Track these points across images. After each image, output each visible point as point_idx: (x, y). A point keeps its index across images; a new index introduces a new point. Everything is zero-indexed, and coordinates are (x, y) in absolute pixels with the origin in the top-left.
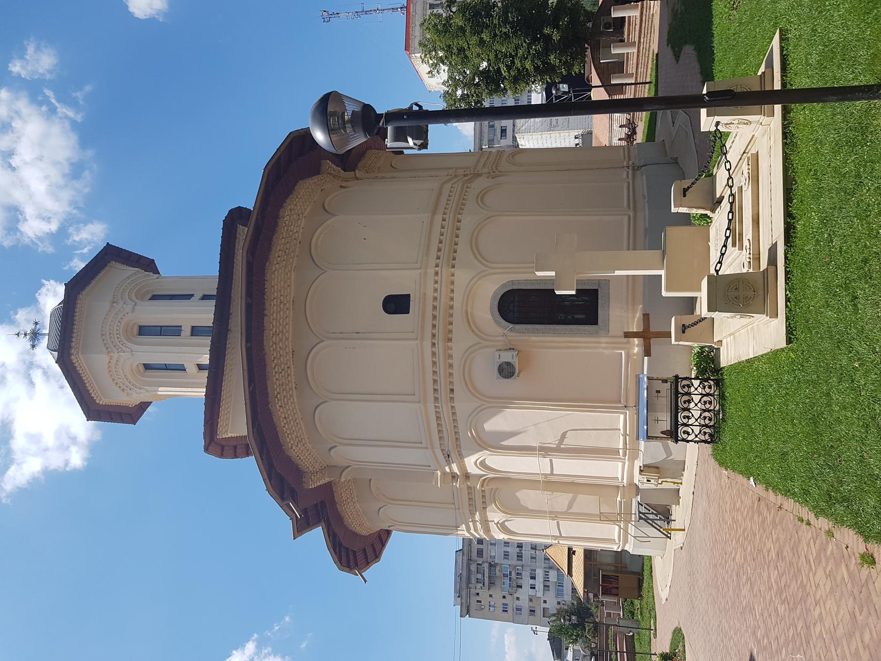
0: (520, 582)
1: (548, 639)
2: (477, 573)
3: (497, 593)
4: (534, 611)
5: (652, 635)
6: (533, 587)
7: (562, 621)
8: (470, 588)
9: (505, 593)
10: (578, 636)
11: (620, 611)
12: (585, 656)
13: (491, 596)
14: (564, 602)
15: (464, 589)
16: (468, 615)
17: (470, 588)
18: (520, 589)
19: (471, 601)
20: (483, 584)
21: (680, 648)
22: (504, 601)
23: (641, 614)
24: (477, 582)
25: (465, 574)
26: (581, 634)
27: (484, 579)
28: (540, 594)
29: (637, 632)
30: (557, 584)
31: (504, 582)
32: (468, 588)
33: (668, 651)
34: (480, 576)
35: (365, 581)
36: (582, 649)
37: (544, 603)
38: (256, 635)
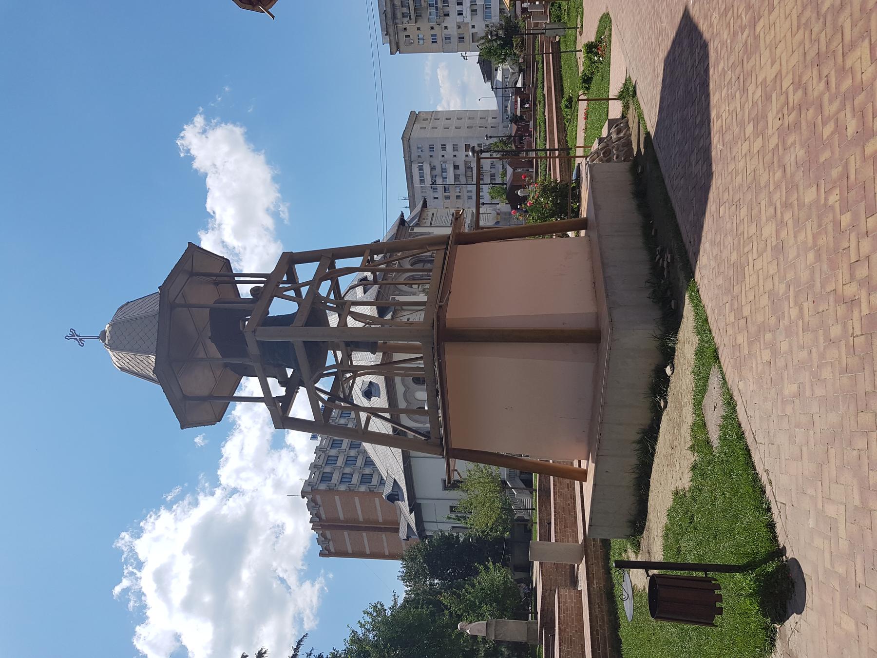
0: (447, 10)
1: (478, 62)
2: (402, 7)
3: (425, 25)
4: (463, 38)
5: (578, 33)
6: (460, 14)
7: (489, 37)
8: (396, 24)
9: (433, 24)
10: (506, 55)
11: (547, 20)
12: (513, 73)
13: (419, 29)
14: (492, 24)
15: (390, 26)
16: (398, 52)
17: (396, 24)
18: (447, 18)
19: (399, 37)
20: (410, 18)
21: (607, 33)
22: (433, 32)
23: (568, 15)
24: (403, 17)
25: (389, 10)
26: (509, 53)
27: (410, 12)
28: (468, 19)
29: (563, 34)
30: (485, 6)
31: (430, 13)
32: (395, 24)
33: (593, 40)
34: (405, 10)
35: (273, 17)
36: (511, 68)
37: (472, 28)
38: (201, 109)
